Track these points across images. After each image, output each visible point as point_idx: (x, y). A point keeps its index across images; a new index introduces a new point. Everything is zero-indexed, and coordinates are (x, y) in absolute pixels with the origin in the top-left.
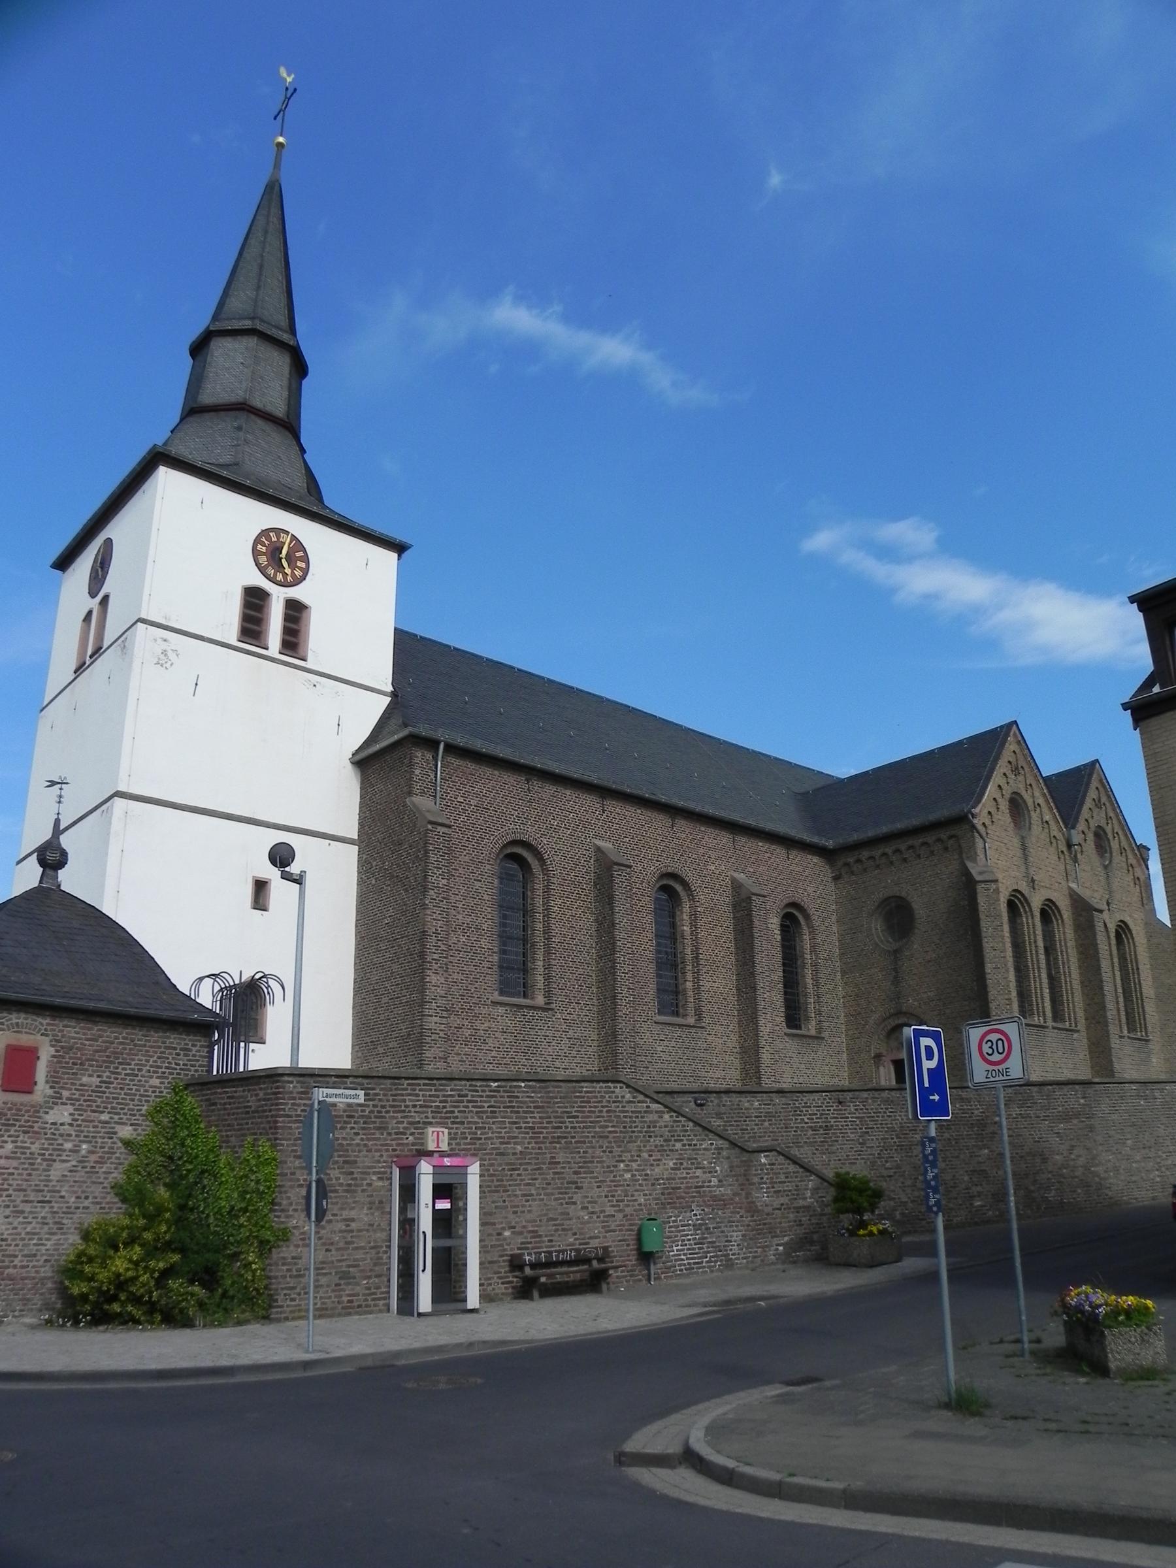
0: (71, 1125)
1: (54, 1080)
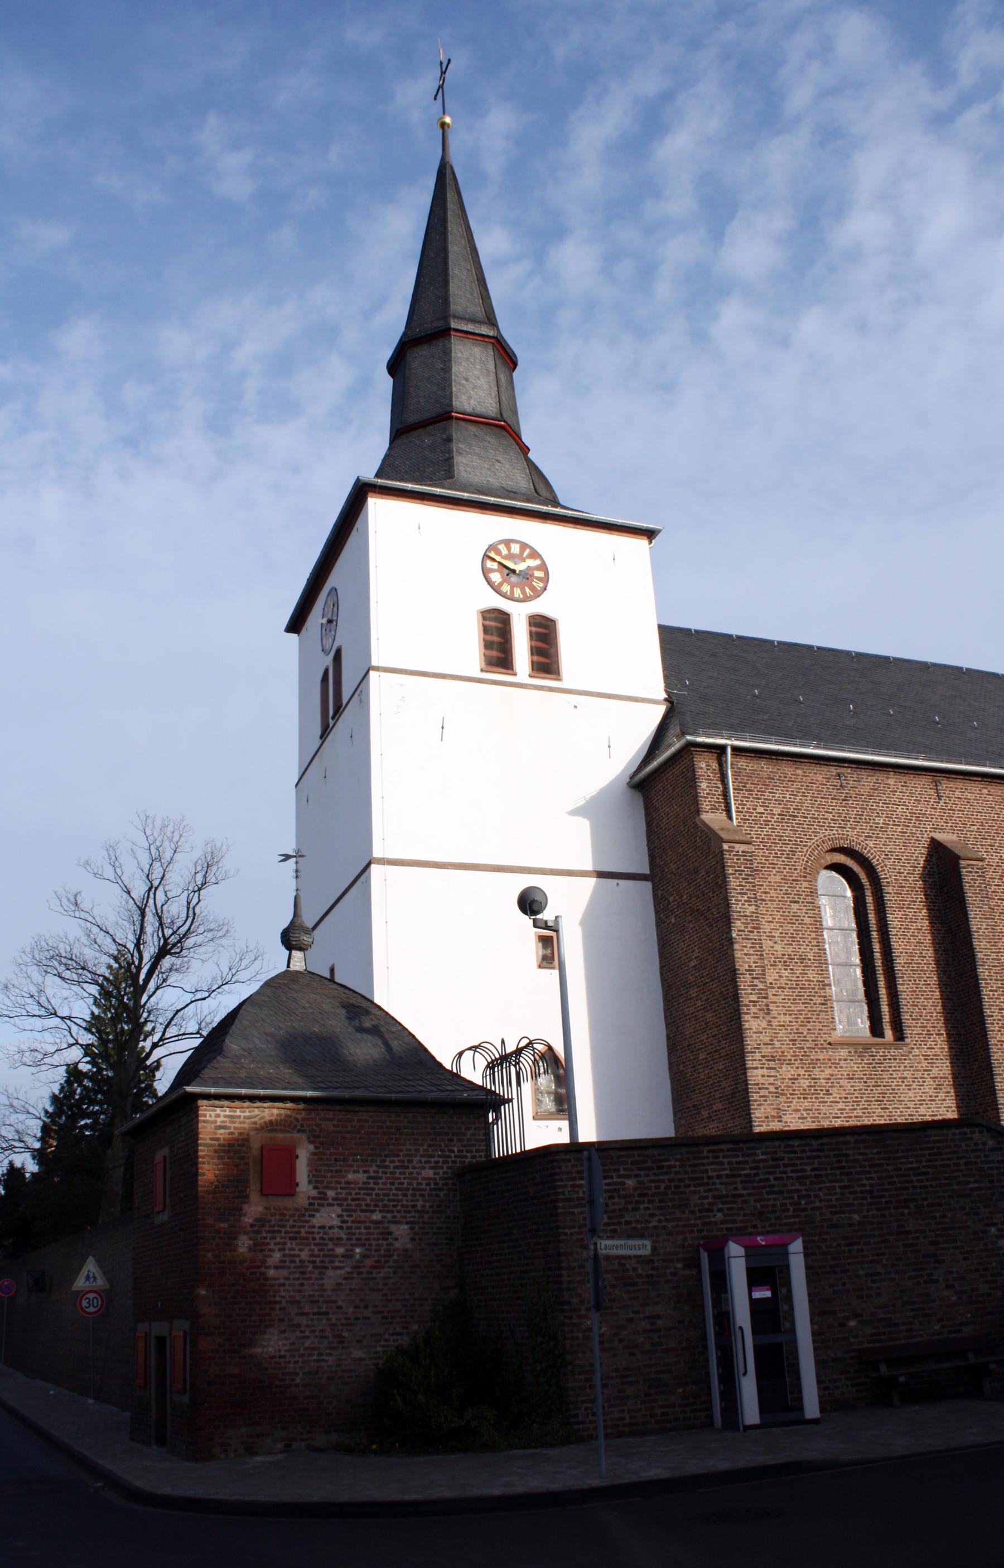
0: (341, 1228)
1: (316, 1178)
